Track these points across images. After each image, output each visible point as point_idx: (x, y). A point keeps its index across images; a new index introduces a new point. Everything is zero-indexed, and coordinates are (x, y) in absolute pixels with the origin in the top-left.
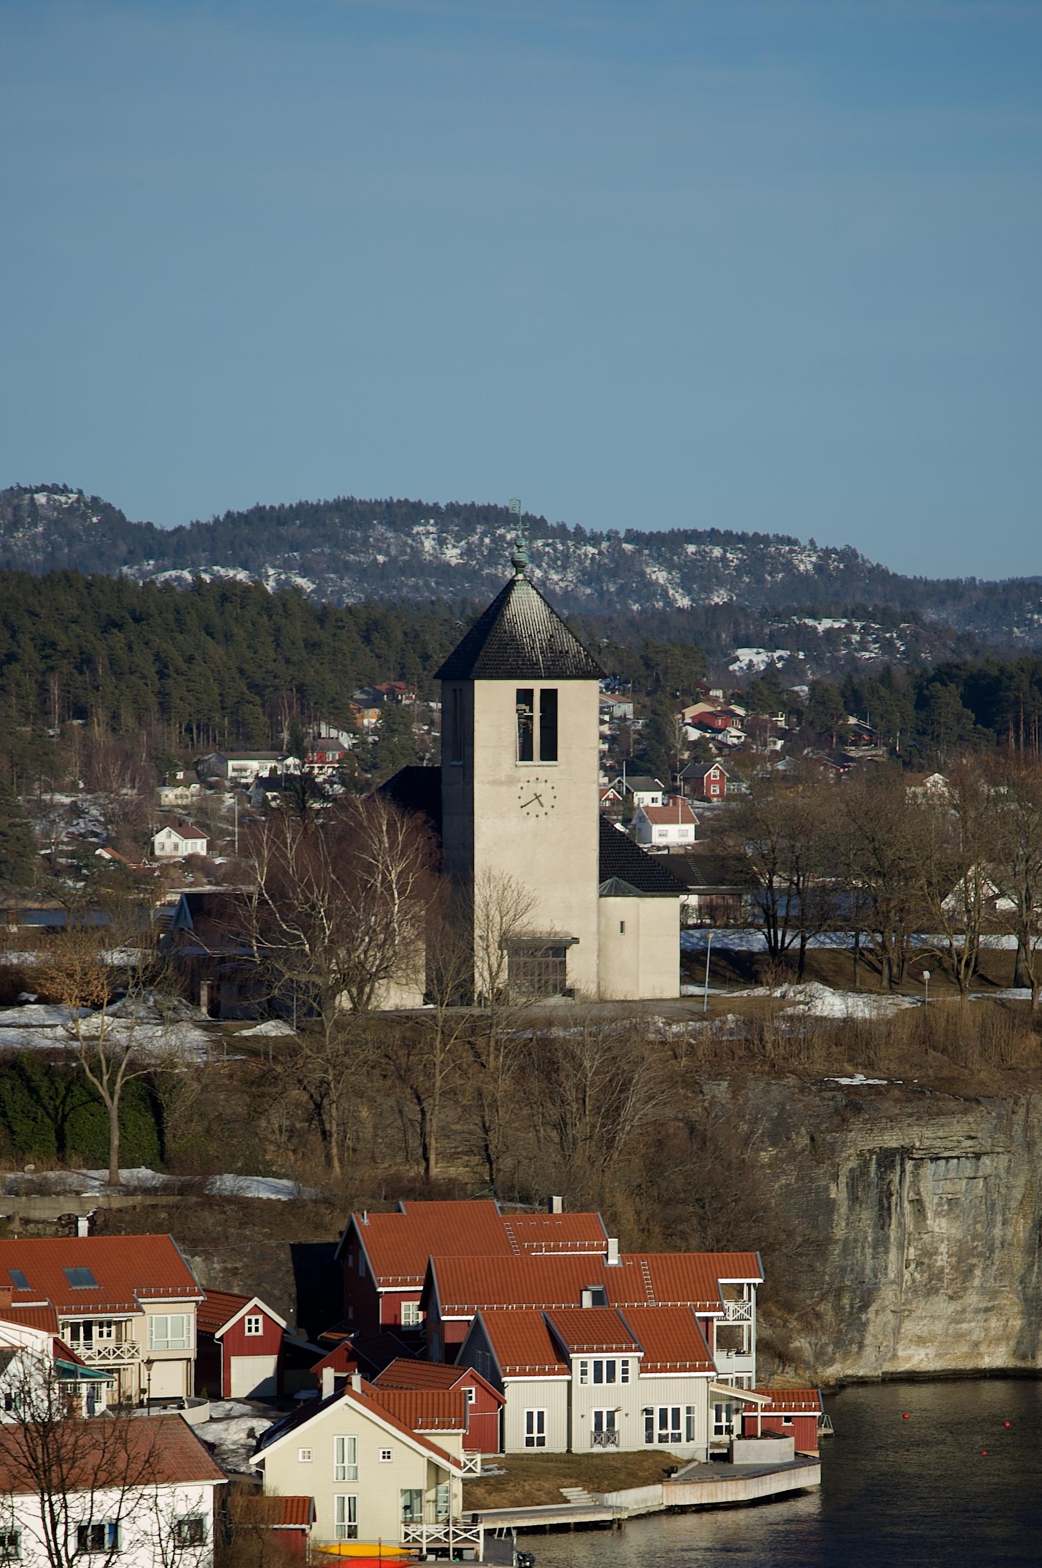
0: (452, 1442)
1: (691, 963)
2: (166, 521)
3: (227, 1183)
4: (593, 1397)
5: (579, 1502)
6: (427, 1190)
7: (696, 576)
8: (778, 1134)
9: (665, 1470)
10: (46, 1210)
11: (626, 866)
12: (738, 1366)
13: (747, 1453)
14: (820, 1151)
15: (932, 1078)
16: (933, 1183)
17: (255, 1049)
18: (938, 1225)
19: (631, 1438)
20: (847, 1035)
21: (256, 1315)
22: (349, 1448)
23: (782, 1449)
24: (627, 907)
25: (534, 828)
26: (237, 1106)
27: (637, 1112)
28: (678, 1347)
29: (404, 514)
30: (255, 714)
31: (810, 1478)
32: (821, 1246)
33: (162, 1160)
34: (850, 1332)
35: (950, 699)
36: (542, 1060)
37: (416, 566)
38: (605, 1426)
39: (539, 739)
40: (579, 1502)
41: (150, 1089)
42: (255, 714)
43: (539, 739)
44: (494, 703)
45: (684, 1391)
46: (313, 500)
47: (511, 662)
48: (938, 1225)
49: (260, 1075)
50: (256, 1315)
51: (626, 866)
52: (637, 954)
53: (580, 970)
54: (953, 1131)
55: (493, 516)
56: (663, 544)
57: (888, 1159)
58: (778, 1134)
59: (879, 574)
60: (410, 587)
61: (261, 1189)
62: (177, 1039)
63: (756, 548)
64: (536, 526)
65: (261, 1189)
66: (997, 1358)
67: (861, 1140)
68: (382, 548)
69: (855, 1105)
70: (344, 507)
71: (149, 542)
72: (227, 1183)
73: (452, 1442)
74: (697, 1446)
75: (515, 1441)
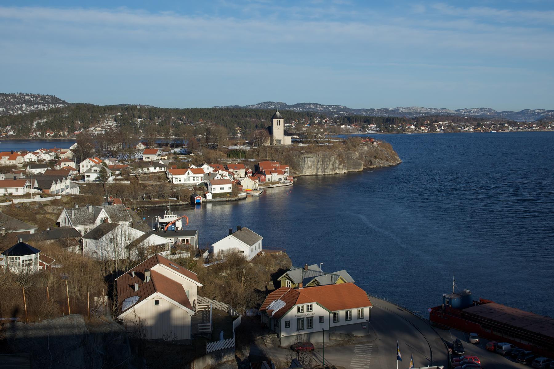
0: (257, 181)
1: (292, 142)
2: (290, 105)
3: (249, 160)
4: (274, 177)
5: (271, 186)
6: (266, 160)
7: (333, 109)
8: (296, 156)
9: (279, 183)
10: (234, 162)
11: (286, 133)
12: (287, 174)
13: (286, 181)
14: (299, 157)
15: (309, 151)
16: (309, 159)
17: (254, 149)
18: (309, 163)
19: (277, 180)
20: (302, 148)
21: (250, 170)
22: (247, 181)
23: (289, 181)
24: (286, 137)
25: (278, 131)
26: (252, 153)
27: (284, 154)
28: (280, 173)
29: (309, 104)
30: (288, 121)
31: (292, 183)
32: (299, 165)
33: (245, 158)
34: (302, 171)
35: (346, 119)
36: (276, 149)
37: (310, 108)
38: (275, 179)
39: (279, 124)
40: (271, 186)
41: (244, 152)
42: (288, 121)
43: (279, 124)
44: (275, 121)
45: (281, 176)
46: (202, 108)
47: (276, 118)
48: (309, 163)
49: (253, 151)
50: (250, 170)
51: (286, 133)
52: (288, 141)
53: (282, 142)
54: (310, 155)
55: (316, 104)
56: (331, 106)
57: (305, 158)
58: (296, 156)
59: (348, 108)
60: (309, 110)
61: (252, 160)
62: (248, 148)
63: (338, 107)
64: (320, 105)
65: (252, 160)
66: (314, 174)
67: (303, 156)
68: (307, 106)
69: (302, 153)
70: (304, 103)
71: (289, 106)
72: (249, 160)
73: (257, 181)
74: (282, 181)
75: (267, 181)
